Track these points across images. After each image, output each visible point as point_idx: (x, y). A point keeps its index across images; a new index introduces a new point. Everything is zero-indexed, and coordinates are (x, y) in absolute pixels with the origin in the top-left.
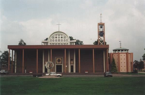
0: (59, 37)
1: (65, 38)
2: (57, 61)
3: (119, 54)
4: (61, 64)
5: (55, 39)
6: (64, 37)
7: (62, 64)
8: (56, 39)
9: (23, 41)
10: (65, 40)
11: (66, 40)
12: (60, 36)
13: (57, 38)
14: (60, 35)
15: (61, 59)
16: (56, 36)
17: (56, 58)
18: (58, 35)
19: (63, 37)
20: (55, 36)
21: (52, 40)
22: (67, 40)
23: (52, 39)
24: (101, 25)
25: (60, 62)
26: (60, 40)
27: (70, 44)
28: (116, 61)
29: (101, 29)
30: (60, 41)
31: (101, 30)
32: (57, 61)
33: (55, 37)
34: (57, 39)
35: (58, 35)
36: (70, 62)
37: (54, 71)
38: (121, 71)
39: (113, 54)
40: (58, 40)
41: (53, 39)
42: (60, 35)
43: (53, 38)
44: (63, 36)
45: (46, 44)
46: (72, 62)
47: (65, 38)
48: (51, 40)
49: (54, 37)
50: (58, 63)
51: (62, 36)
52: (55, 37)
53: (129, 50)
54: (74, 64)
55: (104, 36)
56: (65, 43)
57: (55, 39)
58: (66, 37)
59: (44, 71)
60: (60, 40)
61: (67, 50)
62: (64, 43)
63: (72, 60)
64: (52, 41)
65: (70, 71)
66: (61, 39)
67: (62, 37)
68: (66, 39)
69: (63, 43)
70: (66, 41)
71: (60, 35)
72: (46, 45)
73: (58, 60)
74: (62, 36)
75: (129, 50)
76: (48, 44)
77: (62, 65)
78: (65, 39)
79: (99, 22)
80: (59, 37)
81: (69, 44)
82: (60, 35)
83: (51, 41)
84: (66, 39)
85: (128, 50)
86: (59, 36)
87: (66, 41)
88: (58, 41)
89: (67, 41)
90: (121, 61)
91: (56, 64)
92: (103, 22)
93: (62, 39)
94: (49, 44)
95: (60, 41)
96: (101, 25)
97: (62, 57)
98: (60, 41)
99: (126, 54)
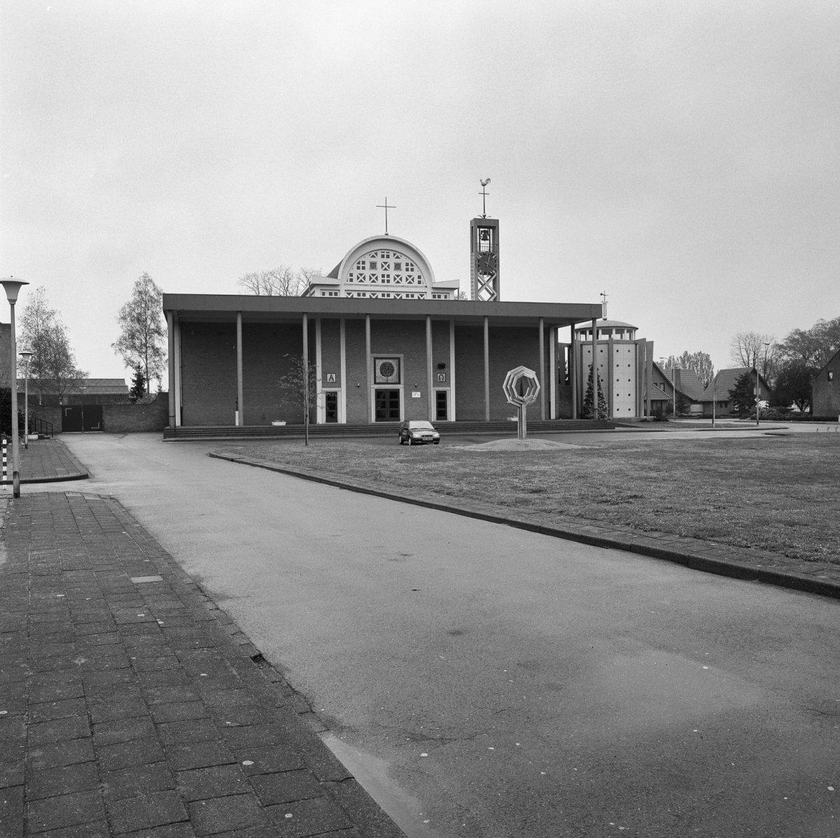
0: (385, 266)
1: (410, 267)
2: (378, 371)
3: (609, 343)
4: (398, 384)
5: (368, 272)
6: (407, 264)
7: (399, 383)
8: (373, 272)
9: (151, 281)
10: (374, 279)
11: (416, 280)
12: (392, 261)
13: (379, 266)
14: (388, 257)
15: (394, 363)
16: (373, 260)
17: (399, 359)
18: (383, 256)
19: (403, 267)
20: (368, 260)
21: (355, 277)
22: (419, 277)
23: (356, 272)
24: (485, 228)
25: (390, 378)
26: (388, 276)
27: (434, 296)
28: (601, 372)
29: (482, 242)
30: (392, 282)
31: (485, 246)
32: (378, 371)
33: (367, 265)
34: (379, 272)
35: (380, 254)
36: (324, 378)
37: (426, 418)
38: (616, 415)
39: (581, 345)
40: (380, 279)
41: (361, 271)
42: (391, 254)
43: (358, 268)
44: (403, 261)
45: (331, 294)
46: (442, 377)
47: (412, 270)
48: (351, 275)
49: (364, 263)
50: (384, 379)
51: (398, 257)
52: (367, 265)
53: (637, 329)
54: (338, 384)
55: (497, 271)
56: (386, 289)
57: (368, 272)
58: (415, 267)
59: (435, 418)
60: (391, 279)
61: (441, 325)
62: (407, 290)
63: (441, 367)
64: (355, 281)
65: (321, 418)
66: (392, 272)
67: (398, 267)
68: (415, 274)
69: (403, 289)
70: (416, 283)
71: (391, 254)
72: (327, 295)
73: (381, 369)
74: (398, 261)
75: (637, 329)
76: (336, 294)
77: (401, 387)
78: (410, 273)
79: (478, 214)
80: (385, 266)
81: (429, 297)
82: (388, 257)
83: (351, 280)
84: (415, 274)
85: (632, 330)
86: (385, 260)
87: (416, 283)
88: (383, 281)
89: (419, 282)
90: (617, 373)
91: (375, 383)
92: (491, 215)
93: (398, 273)
94: (343, 294)
95: (392, 282)
96: (485, 228)
97: (401, 356)
98: (388, 281)
99: (636, 345)
